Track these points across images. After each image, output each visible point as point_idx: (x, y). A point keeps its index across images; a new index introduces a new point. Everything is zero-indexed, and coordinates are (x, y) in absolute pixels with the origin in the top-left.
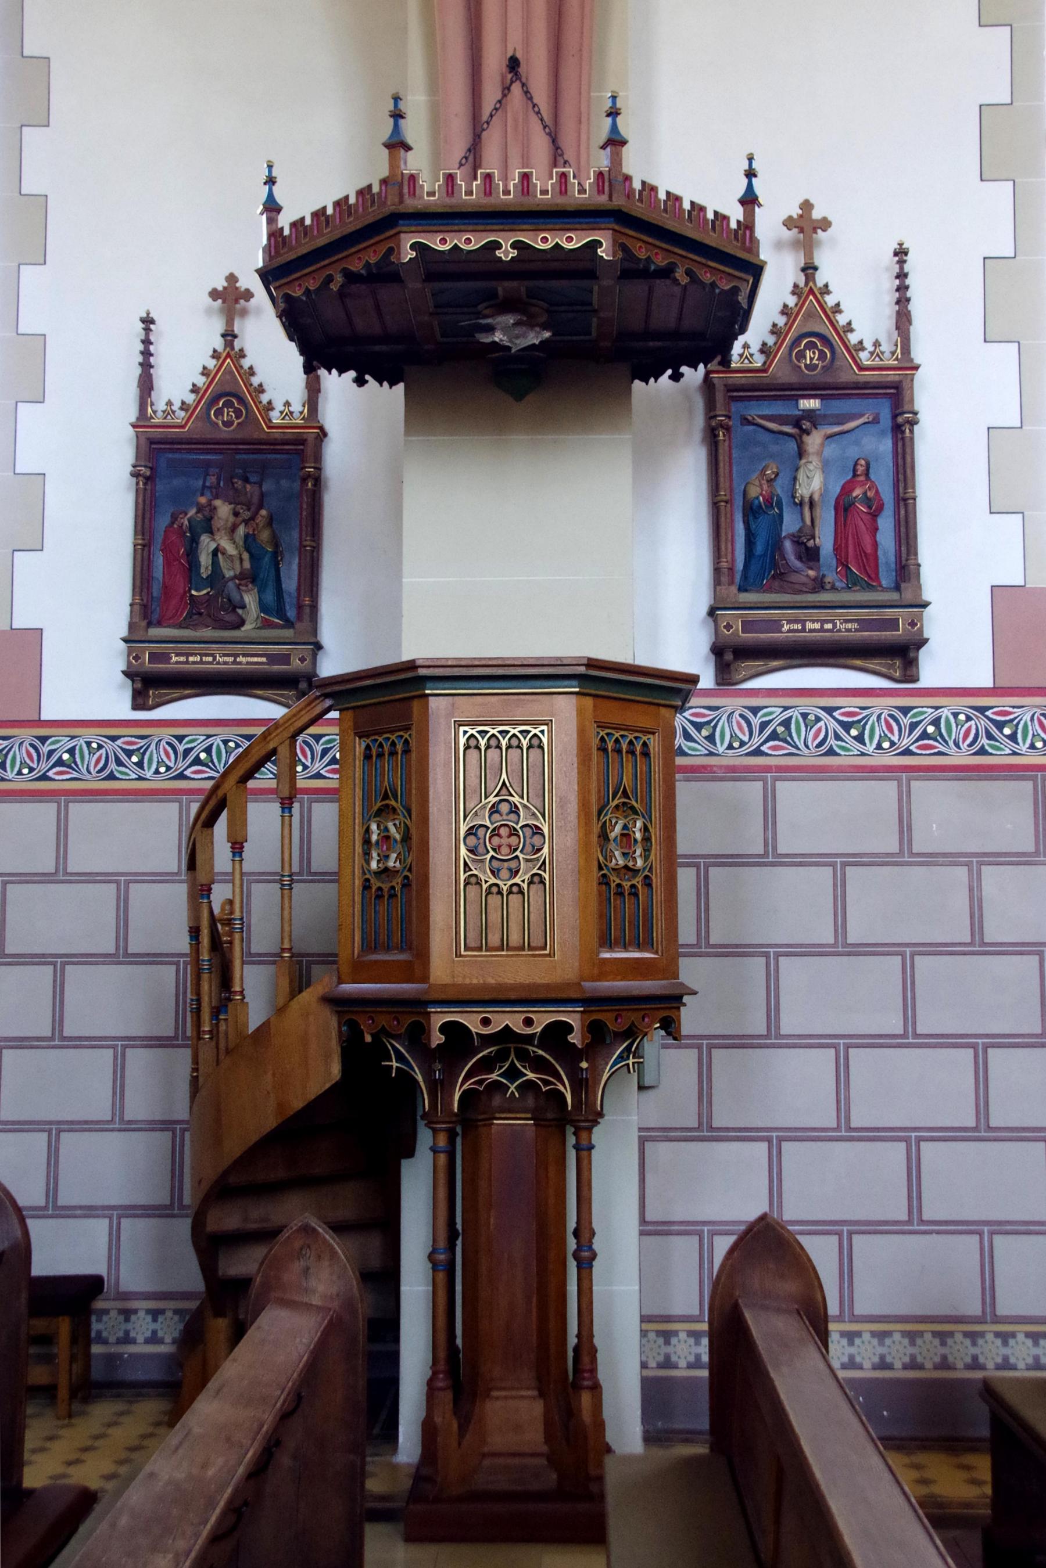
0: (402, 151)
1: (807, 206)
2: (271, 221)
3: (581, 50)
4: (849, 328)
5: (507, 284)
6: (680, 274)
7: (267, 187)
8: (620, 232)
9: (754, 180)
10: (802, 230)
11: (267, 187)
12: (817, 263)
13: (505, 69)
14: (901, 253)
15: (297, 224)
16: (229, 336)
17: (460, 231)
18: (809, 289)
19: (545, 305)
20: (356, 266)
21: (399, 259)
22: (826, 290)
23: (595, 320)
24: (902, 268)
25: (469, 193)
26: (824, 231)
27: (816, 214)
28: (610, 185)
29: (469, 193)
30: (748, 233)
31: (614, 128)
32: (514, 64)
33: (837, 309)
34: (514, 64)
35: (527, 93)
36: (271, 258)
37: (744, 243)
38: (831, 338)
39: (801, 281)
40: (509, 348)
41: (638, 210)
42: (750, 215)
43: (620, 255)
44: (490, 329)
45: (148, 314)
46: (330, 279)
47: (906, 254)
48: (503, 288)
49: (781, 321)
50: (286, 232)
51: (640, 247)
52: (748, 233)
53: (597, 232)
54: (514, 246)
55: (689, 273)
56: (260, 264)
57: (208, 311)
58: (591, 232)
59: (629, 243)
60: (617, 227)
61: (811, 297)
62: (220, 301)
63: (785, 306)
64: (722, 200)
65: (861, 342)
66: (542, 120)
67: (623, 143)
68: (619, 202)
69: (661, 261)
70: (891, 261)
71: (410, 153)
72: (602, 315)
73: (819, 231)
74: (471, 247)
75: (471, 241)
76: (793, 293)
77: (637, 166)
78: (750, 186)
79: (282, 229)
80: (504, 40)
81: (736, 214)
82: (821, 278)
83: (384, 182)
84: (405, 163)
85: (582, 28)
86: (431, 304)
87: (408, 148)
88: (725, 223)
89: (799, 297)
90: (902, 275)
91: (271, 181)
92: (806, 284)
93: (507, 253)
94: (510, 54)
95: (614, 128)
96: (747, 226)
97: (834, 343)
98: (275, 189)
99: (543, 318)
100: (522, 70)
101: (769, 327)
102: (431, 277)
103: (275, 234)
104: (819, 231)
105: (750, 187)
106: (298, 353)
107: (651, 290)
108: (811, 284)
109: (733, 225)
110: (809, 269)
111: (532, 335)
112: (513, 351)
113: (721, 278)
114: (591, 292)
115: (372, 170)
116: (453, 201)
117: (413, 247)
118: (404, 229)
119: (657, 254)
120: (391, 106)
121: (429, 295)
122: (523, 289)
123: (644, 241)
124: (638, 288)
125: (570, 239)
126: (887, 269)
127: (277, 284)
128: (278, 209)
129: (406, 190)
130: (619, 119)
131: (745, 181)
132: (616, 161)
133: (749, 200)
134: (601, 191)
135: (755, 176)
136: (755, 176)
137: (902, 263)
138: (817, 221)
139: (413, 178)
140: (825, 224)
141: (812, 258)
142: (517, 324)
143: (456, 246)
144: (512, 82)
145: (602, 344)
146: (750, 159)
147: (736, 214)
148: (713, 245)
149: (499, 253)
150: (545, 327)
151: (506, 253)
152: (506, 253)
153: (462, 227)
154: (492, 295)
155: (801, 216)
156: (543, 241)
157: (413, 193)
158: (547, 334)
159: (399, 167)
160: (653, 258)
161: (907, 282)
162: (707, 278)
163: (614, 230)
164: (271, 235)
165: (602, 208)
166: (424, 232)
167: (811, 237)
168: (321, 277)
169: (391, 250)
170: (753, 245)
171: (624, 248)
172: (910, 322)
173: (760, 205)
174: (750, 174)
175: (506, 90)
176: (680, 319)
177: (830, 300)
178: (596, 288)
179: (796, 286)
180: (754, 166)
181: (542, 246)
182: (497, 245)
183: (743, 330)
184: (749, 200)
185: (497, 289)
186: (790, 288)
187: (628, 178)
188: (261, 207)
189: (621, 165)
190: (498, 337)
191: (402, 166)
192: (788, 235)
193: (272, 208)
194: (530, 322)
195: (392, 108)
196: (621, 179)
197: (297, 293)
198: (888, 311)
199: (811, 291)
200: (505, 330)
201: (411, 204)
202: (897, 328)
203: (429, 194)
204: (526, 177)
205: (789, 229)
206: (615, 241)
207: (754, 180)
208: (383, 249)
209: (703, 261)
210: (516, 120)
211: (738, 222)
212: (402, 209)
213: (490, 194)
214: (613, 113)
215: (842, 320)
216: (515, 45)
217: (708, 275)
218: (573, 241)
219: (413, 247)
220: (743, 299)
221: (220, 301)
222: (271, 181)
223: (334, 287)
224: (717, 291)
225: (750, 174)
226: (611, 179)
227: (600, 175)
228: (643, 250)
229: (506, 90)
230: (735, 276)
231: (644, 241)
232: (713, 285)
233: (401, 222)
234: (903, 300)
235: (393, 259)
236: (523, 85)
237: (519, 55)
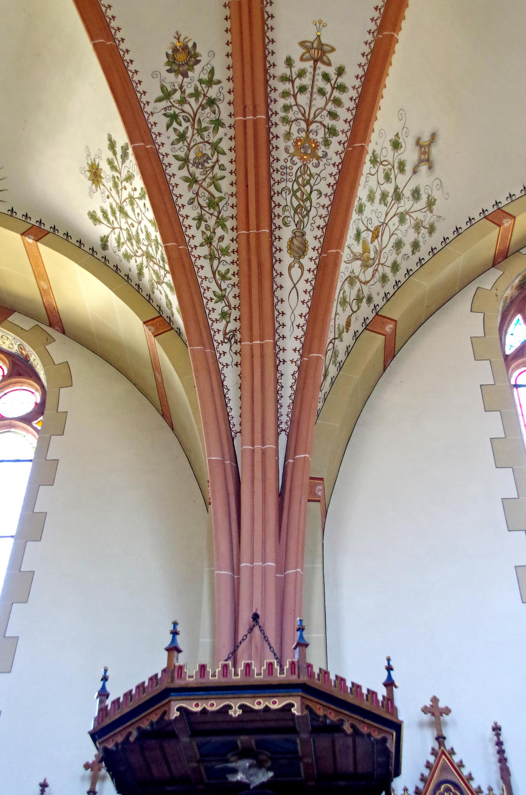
0: (176, 653)
1: (435, 700)
2: (101, 702)
3: (295, 611)
4: (470, 778)
5: (244, 738)
6: (347, 727)
7: (102, 682)
8: (306, 698)
9: (392, 672)
10: (433, 714)
11: (102, 682)
12: (445, 734)
13: (251, 620)
14: (497, 729)
15: (116, 702)
16: (440, 739)
17: (207, 699)
18: (442, 751)
19: (269, 755)
20: (145, 725)
21: (169, 717)
22: (452, 752)
23: (302, 765)
24: (499, 738)
25: (214, 675)
26: (447, 714)
27: (442, 705)
28: (299, 669)
29: (214, 675)
30: (389, 702)
31: (301, 637)
32: (256, 617)
33: (461, 765)
34: (256, 617)
35: (262, 630)
36: (99, 724)
37: (388, 709)
38: (459, 784)
39: (436, 746)
40: (248, 785)
41: (317, 684)
42: (390, 693)
43: (306, 712)
44: (235, 771)
45: (45, 780)
46: (130, 734)
47: (500, 730)
48: (241, 740)
49: (426, 772)
50: (109, 708)
51: (319, 708)
52: (389, 702)
53: (291, 698)
54: (241, 707)
55: (353, 726)
56: (91, 728)
57: (83, 778)
58: (287, 698)
59: (311, 705)
60: (304, 695)
61: (443, 756)
62: (90, 770)
63: (428, 762)
64: (372, 681)
65: (479, 788)
66: (269, 644)
67: (307, 645)
68: (304, 679)
69: (333, 717)
70: (491, 734)
71: (180, 654)
72: (305, 760)
73: (444, 715)
74: (214, 708)
75: (214, 705)
76: (433, 754)
77: (316, 659)
78: (389, 676)
79: (107, 707)
80: (252, 602)
81: (382, 692)
82: (449, 744)
83: (164, 671)
84: (177, 659)
85: (295, 596)
86: (198, 754)
87: (179, 651)
88: (374, 695)
89: (436, 756)
90: (499, 743)
91: (105, 679)
92: (440, 748)
93: (235, 712)
94: (254, 612)
95: (301, 637)
96: (389, 699)
97: (462, 787)
98: (107, 684)
99: (269, 764)
100: (261, 620)
101: (419, 776)
102: (194, 733)
103: (103, 711)
104: (444, 715)
105: (389, 676)
106: (115, 792)
107: (333, 741)
108: (442, 748)
109: (380, 698)
110: (440, 739)
111: (260, 775)
112: (251, 787)
113: (374, 731)
114: (296, 744)
115: (158, 664)
116: (203, 680)
117: (179, 709)
118: (173, 698)
119: (330, 713)
120: (171, 628)
121: (195, 747)
122: (253, 741)
123: (321, 704)
124: (324, 741)
125: (274, 703)
126: (490, 740)
127: (101, 740)
128: (107, 696)
129: (176, 675)
130: (304, 633)
131: (386, 673)
132: (303, 656)
133: (389, 684)
134: (293, 672)
135: (392, 669)
136: (392, 669)
137: (498, 735)
138: (442, 709)
139: (181, 668)
140: (447, 711)
141: (441, 731)
142: (250, 766)
143: (204, 709)
144: (254, 626)
145: (309, 783)
146: (389, 660)
147: (382, 692)
148: (367, 709)
149: (231, 712)
150: (269, 769)
151: (235, 712)
152: (235, 712)
153: (209, 696)
154: (232, 747)
155: (432, 706)
156: (258, 704)
157: (180, 676)
158: (271, 774)
159: (173, 661)
160: (328, 715)
161: (503, 747)
162: (365, 730)
163: (301, 696)
164: (100, 710)
165: (293, 683)
166: (186, 699)
167: (439, 719)
168: (125, 734)
169: (165, 713)
170: (394, 710)
171: (308, 707)
172: (509, 774)
173: (396, 687)
174: (389, 669)
175: (251, 630)
176: (355, 763)
177: (456, 759)
178: (298, 741)
179: (433, 749)
180: (391, 663)
181: (257, 707)
182: (229, 707)
183: (397, 773)
184: (389, 684)
185: (236, 742)
186: (430, 750)
187: (309, 666)
188: (97, 693)
189: (305, 657)
190: (240, 777)
191: (175, 661)
192: (428, 717)
193: (103, 694)
194: (260, 765)
195: (172, 628)
196: (305, 666)
197: (111, 746)
198: (495, 767)
199: (443, 753)
200: (244, 772)
201: (178, 683)
202: (502, 778)
203: (189, 677)
204: (248, 666)
205: (425, 714)
206: (302, 704)
207: (392, 672)
208: (160, 712)
209: (362, 719)
210: (257, 648)
211: (384, 697)
212: (172, 686)
213: (227, 676)
214: (301, 629)
215: (465, 772)
216: (257, 608)
217: (366, 729)
218: (276, 704)
219: (179, 709)
220: (391, 745)
221: (90, 770)
222: (105, 679)
223: (132, 739)
224: (372, 739)
225: (389, 669)
226: (301, 666)
227: (293, 664)
228: (322, 710)
229: (251, 630)
230: (383, 730)
231: (321, 704)
232: (369, 735)
233: (172, 694)
234: (503, 760)
235: (166, 717)
236: (260, 627)
237: (259, 612)
